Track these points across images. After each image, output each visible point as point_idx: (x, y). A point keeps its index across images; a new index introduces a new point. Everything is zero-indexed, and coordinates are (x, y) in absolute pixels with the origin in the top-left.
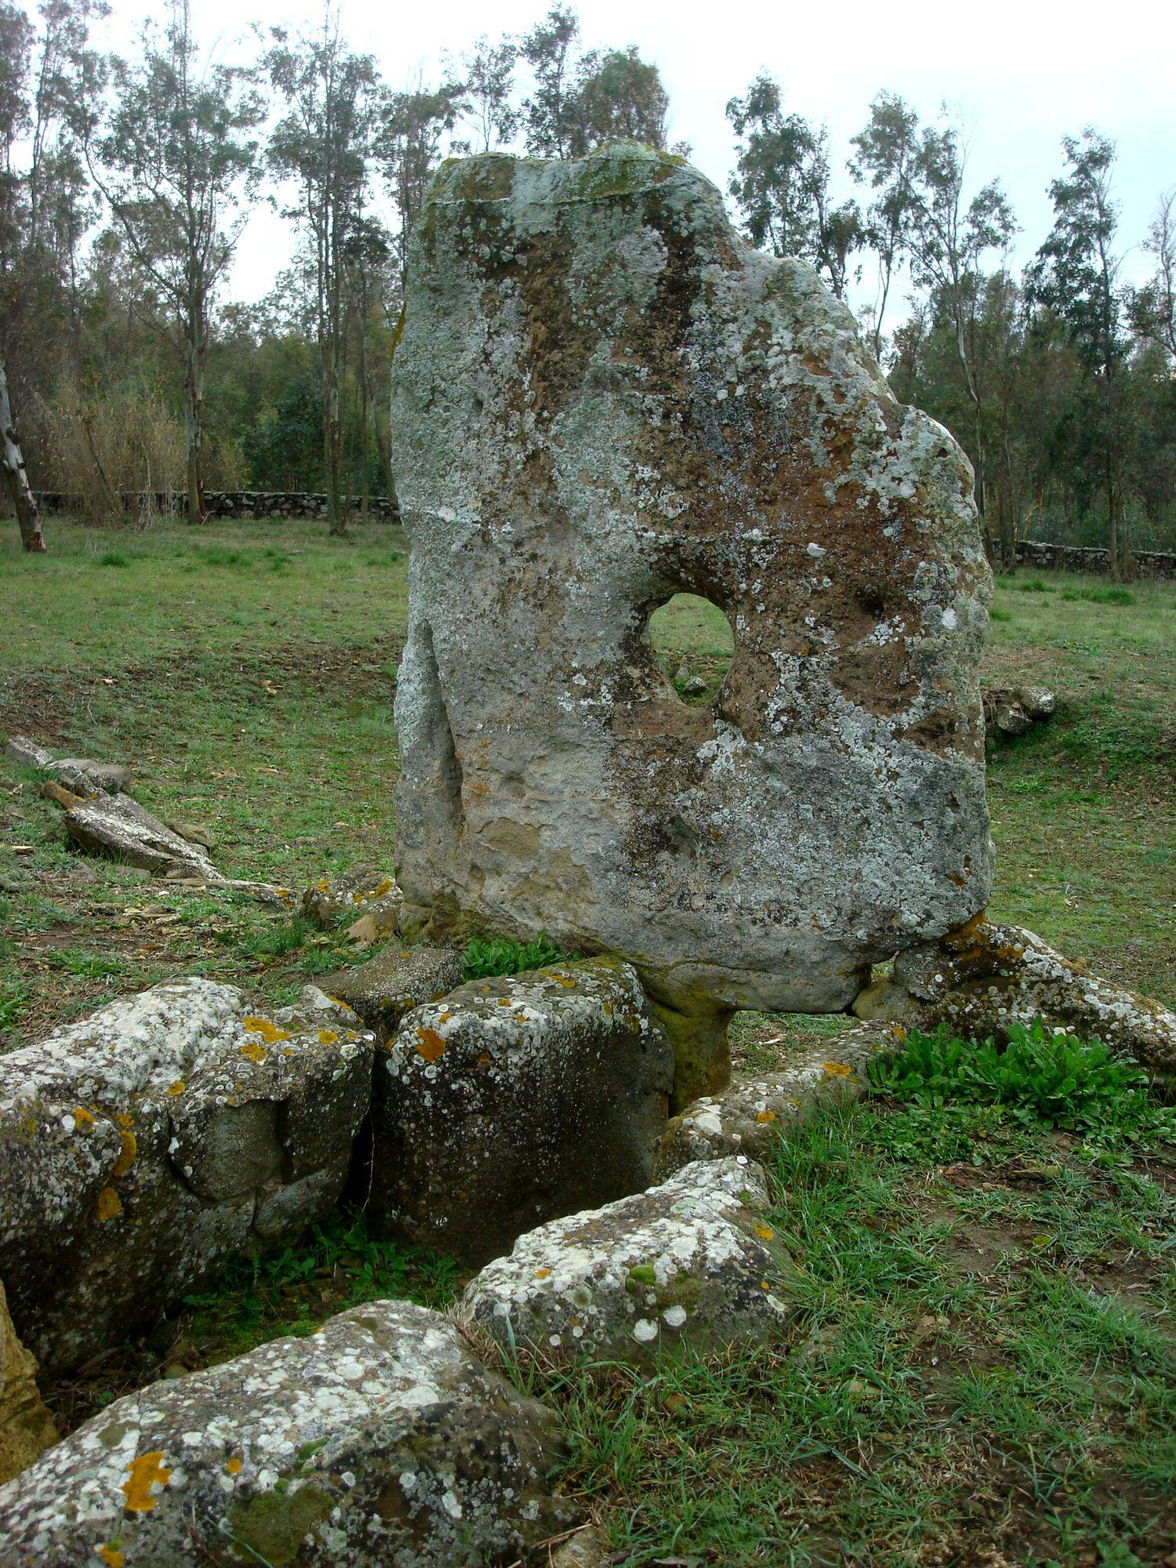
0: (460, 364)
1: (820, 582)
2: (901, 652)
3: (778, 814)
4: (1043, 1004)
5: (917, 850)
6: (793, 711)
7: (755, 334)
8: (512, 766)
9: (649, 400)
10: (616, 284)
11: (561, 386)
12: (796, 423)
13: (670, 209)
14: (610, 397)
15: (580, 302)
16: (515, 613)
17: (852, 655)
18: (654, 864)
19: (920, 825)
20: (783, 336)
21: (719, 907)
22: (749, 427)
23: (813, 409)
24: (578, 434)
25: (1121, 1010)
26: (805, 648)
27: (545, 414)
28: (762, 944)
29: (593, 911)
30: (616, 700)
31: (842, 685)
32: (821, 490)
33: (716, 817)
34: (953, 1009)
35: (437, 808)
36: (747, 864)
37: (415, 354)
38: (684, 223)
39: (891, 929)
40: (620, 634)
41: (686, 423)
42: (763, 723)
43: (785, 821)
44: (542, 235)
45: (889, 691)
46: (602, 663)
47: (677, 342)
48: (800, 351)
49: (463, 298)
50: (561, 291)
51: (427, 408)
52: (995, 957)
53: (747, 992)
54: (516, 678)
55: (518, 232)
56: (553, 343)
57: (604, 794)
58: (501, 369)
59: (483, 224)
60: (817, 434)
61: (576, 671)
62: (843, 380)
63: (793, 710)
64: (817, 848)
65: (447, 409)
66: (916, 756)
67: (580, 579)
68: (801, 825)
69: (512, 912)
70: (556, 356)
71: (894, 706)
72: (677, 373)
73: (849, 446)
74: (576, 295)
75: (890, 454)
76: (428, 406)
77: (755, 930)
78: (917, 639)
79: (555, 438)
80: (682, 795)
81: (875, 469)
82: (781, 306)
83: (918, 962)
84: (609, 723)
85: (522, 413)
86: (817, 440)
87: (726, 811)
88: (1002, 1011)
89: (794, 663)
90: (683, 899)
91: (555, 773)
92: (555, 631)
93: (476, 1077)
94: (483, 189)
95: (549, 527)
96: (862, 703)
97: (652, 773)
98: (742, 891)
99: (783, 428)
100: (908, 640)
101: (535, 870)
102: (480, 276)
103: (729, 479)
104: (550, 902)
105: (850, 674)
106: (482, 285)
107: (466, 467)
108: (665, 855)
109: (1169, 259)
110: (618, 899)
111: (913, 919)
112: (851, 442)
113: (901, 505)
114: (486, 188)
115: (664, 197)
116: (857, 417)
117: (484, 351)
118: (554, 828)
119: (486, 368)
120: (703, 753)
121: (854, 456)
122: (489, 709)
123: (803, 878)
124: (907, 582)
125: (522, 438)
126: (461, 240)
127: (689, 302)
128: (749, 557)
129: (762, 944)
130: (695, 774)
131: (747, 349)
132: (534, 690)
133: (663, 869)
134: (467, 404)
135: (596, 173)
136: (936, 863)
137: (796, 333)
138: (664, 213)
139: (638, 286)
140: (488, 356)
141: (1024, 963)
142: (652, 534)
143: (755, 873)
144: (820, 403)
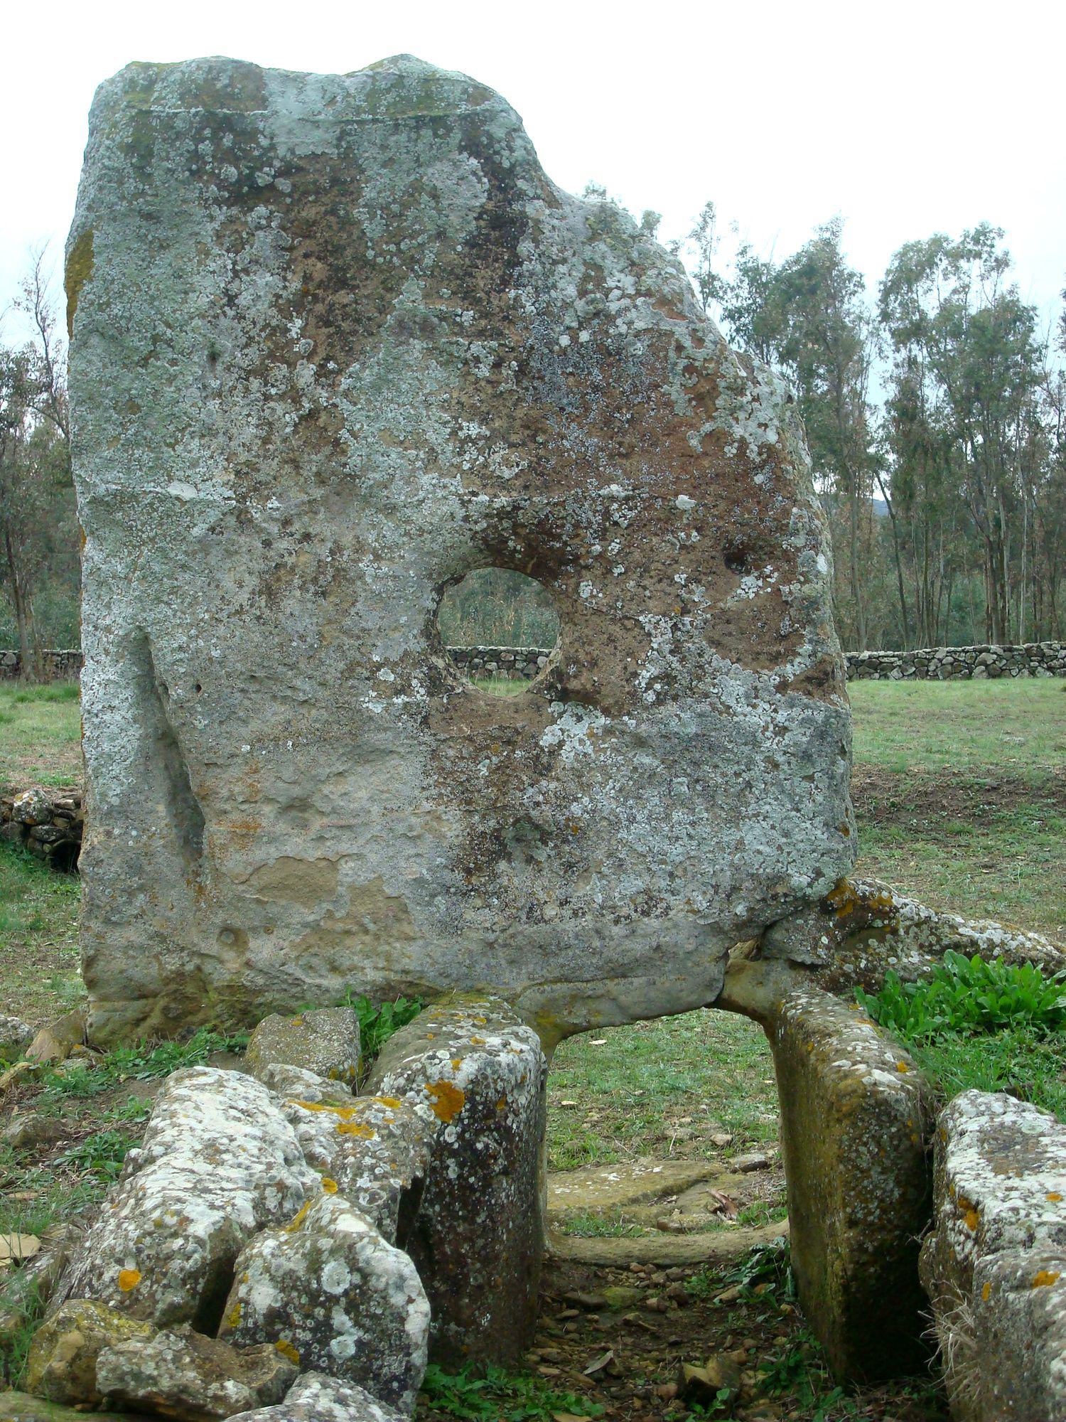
0: (191, 307)
1: (689, 536)
2: (780, 603)
3: (647, 793)
4: (921, 946)
5: (808, 806)
6: (667, 678)
7: (586, 278)
8: (297, 791)
9: (477, 348)
10: (425, 215)
11: (354, 332)
12: (653, 369)
13: (490, 136)
14: (417, 345)
15: (376, 236)
16: (291, 603)
17: (723, 611)
18: (495, 876)
19: (810, 778)
20: (620, 280)
21: (575, 914)
22: (597, 376)
23: (672, 354)
24: (376, 388)
25: (997, 937)
26: (678, 608)
27: (331, 365)
28: (628, 944)
29: (414, 949)
30: (430, 694)
31: (714, 643)
32: (684, 440)
33: (575, 808)
34: (848, 968)
35: (168, 862)
36: (610, 856)
37: (121, 295)
38: (506, 153)
39: (775, 897)
40: (421, 619)
41: (522, 372)
42: (633, 694)
43: (656, 800)
44: (314, 157)
45: (769, 643)
46: (406, 653)
47: (505, 282)
48: (648, 294)
49: (189, 228)
50: (347, 223)
51: (144, 362)
52: (869, 909)
53: (604, 1005)
54: (298, 683)
55: (281, 151)
56: (340, 281)
57: (427, 806)
58: (251, 314)
59: (228, 140)
60: (677, 381)
61: (379, 666)
62: (699, 326)
63: (667, 676)
64: (693, 824)
65: (174, 362)
66: (806, 707)
67: (378, 558)
68: (674, 801)
69: (299, 973)
70: (344, 297)
71: (776, 659)
72: (510, 315)
73: (714, 392)
74: (372, 228)
75: (754, 400)
76: (146, 359)
77: (617, 930)
78: (795, 587)
79: (346, 394)
80: (531, 791)
81: (742, 415)
82: (613, 248)
83: (799, 929)
84: (425, 721)
85: (291, 365)
86: (677, 387)
87: (586, 800)
88: (892, 960)
89: (666, 625)
90: (532, 912)
91: (361, 790)
92: (347, 622)
93: (497, 1129)
94: (225, 97)
95: (325, 499)
96: (738, 660)
97: (484, 771)
98: (603, 889)
99: (638, 375)
100: (785, 589)
101: (330, 915)
102: (217, 202)
103: (574, 432)
104: (351, 952)
105: (728, 632)
106: (221, 214)
107: (208, 432)
108: (503, 865)
109: (44, 319)
110: (451, 927)
111: (805, 880)
112: (715, 387)
113: (769, 451)
114: (232, 96)
115: (483, 122)
116: (719, 363)
117: (226, 292)
118: (359, 856)
119: (231, 313)
120: (547, 740)
121: (719, 402)
122: (255, 725)
123: (678, 860)
124: (782, 529)
125: (294, 395)
126: (196, 156)
127: (516, 239)
128: (607, 514)
129: (628, 944)
130: (542, 764)
131: (582, 293)
132: (322, 694)
133: (505, 881)
134: (200, 357)
135: (388, 91)
136: (827, 816)
137: (638, 276)
138: (484, 140)
139: (454, 219)
140: (232, 300)
141: (897, 909)
142: (483, 498)
143: (621, 865)
144: (680, 348)
